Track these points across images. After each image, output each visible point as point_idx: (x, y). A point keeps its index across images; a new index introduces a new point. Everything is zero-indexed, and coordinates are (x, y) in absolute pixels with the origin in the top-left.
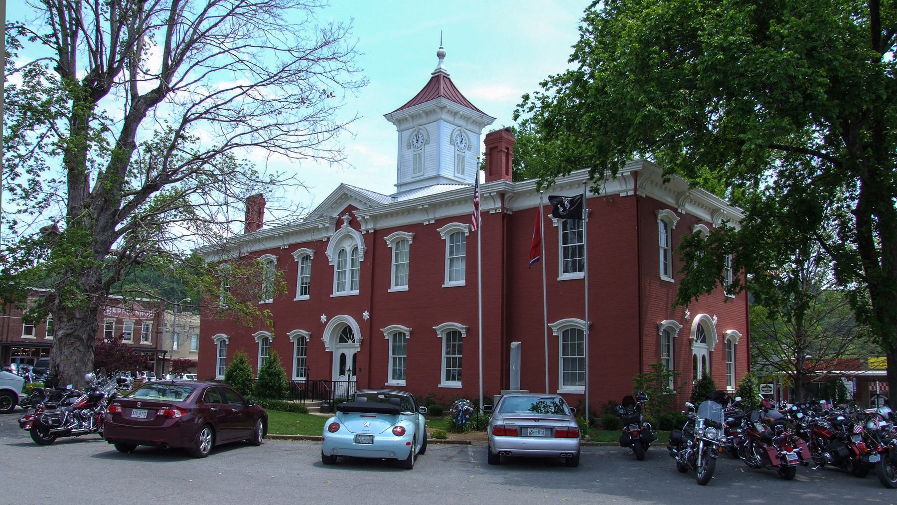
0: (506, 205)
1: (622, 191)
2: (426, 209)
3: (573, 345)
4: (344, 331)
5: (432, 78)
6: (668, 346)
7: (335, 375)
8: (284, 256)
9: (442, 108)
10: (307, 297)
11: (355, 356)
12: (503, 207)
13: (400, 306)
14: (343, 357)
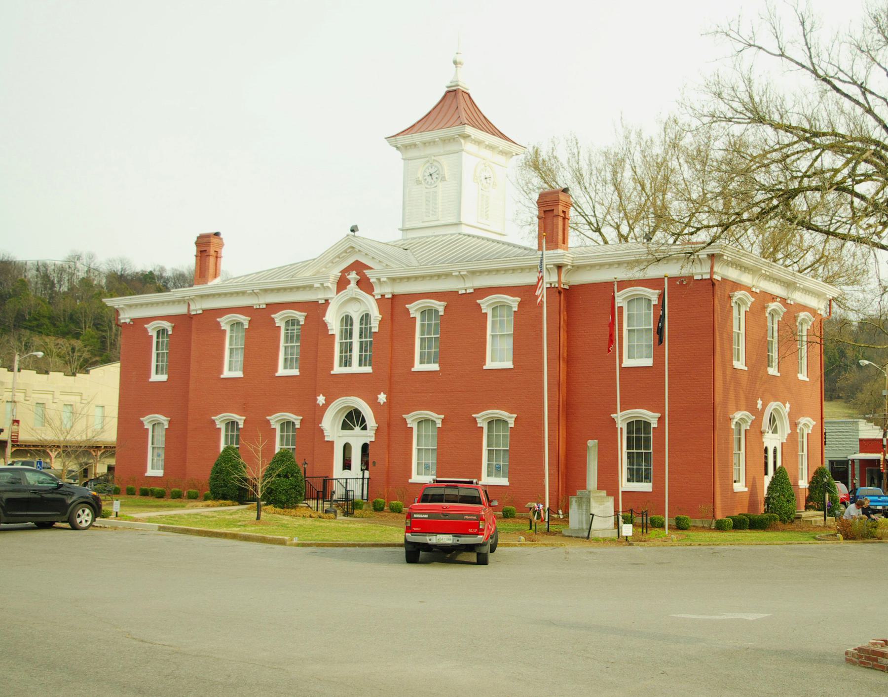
0: (563, 280)
1: (697, 274)
2: (463, 277)
3: (639, 439)
4: (349, 416)
5: (448, 92)
6: (740, 439)
7: (338, 471)
8: (261, 320)
9: (466, 137)
10: (368, 369)
11: (365, 447)
12: (559, 281)
13: (426, 390)
14: (347, 448)
